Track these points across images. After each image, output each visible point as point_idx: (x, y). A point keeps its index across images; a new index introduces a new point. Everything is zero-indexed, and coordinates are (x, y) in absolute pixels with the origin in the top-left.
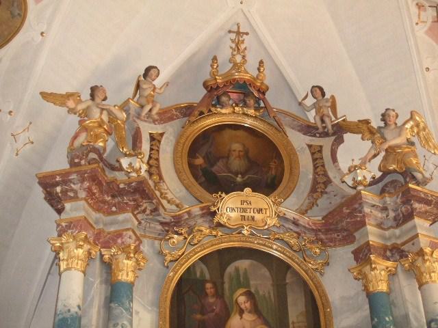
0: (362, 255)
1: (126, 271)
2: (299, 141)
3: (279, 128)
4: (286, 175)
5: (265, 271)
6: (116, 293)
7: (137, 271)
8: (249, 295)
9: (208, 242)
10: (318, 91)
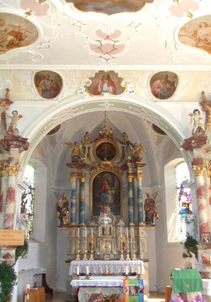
0: (128, 174)
1: (83, 180)
2: (120, 145)
3: (115, 142)
4: (116, 155)
5: (110, 176)
6: (82, 185)
7: (71, 191)
8: (108, 181)
9: (100, 170)
10: (125, 133)
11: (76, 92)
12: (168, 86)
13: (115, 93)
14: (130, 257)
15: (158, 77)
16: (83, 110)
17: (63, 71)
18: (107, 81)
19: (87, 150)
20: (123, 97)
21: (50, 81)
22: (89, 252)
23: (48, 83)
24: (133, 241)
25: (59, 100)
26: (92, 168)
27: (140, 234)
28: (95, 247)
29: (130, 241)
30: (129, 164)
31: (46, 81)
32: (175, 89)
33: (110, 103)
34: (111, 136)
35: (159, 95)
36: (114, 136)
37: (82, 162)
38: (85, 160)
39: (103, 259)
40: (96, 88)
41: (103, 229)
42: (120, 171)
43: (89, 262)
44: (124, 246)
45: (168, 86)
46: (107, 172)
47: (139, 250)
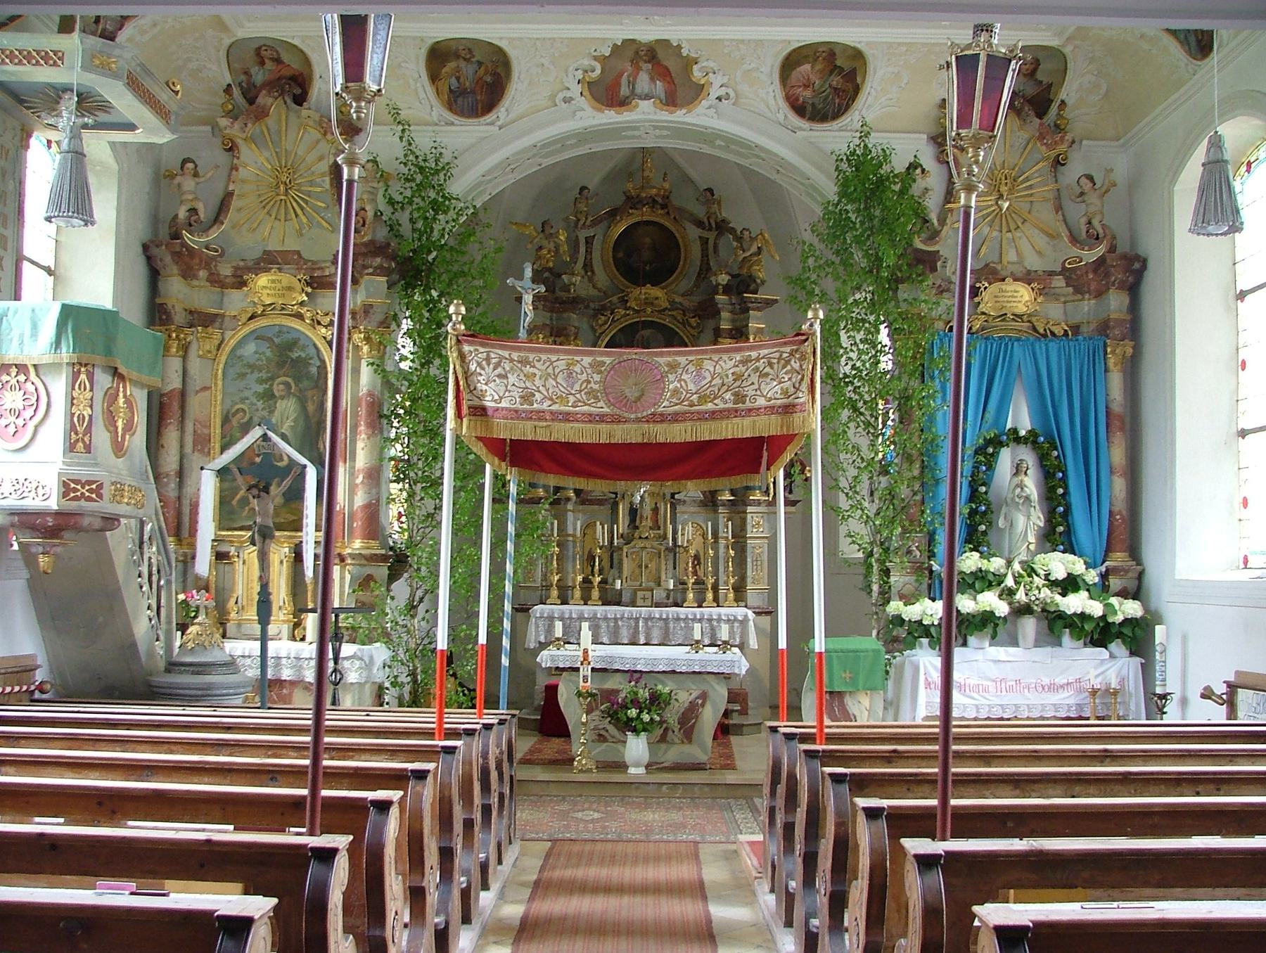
10: (710, 191)
11: (553, 97)
12: (836, 81)
13: (671, 101)
14: (716, 599)
15: (806, 57)
16: (572, 146)
17: (511, 40)
18: (650, 66)
19: (582, 249)
20: (700, 116)
21: (475, 65)
22: (586, 581)
23: (468, 70)
24: (726, 551)
25: (499, 123)
26: (600, 311)
27: (749, 528)
28: (606, 564)
29: (716, 550)
30: (721, 298)
31: (463, 64)
32: (857, 90)
33: (655, 128)
34: (663, 203)
35: (809, 108)
36: (676, 201)
37: (566, 288)
38: (577, 282)
39: (633, 604)
40: (616, 84)
41: (633, 513)
42: (693, 321)
43: (587, 610)
44: (699, 564)
45: (836, 81)
46: (651, 324)
47: (743, 578)
